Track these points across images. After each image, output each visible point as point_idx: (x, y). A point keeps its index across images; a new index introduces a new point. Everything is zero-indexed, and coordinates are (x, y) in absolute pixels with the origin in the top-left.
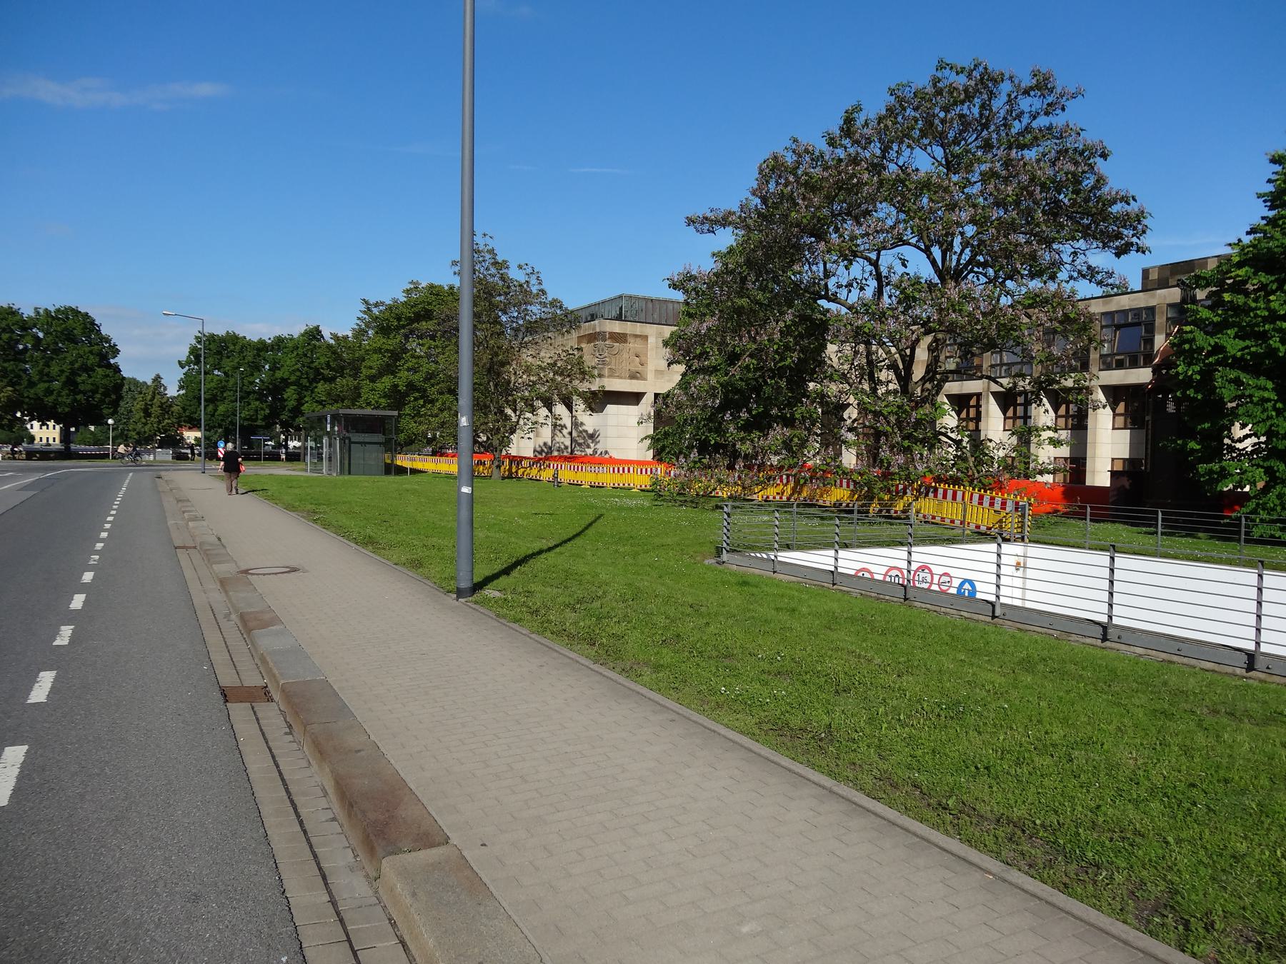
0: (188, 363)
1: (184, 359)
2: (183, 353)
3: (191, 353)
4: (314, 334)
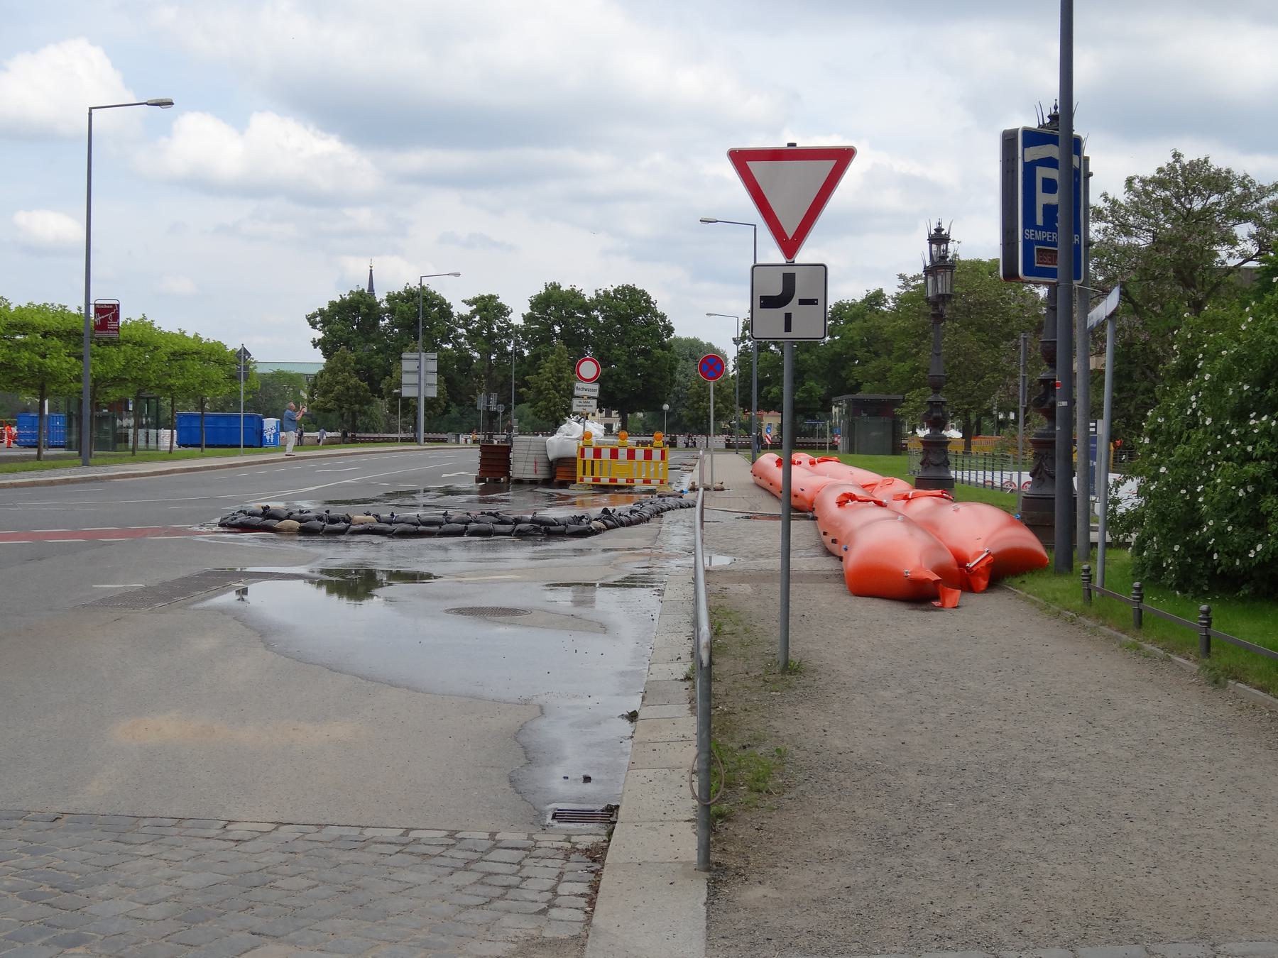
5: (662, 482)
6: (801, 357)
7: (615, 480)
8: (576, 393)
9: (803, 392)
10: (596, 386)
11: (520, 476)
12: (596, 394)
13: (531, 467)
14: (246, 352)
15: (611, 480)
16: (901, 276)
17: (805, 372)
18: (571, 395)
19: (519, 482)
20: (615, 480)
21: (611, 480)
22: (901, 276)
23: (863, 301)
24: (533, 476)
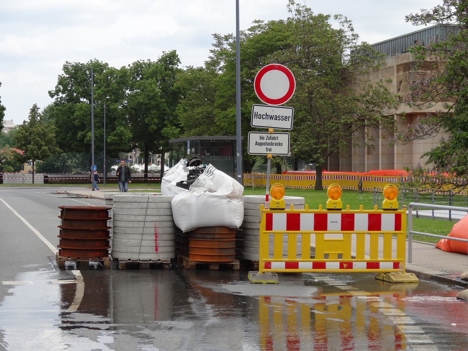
0: (57, 92)
1: (53, 89)
2: (53, 85)
3: (60, 83)
4: (171, 59)
5: (396, 265)
6: (112, 107)
7: (295, 265)
8: (256, 122)
9: (114, 135)
10: (289, 112)
11: (134, 257)
12: (288, 125)
13: (149, 242)
14: (364, 43)
15: (288, 265)
16: (216, 36)
17: (115, 119)
18: (248, 128)
19: (134, 267)
20: (295, 265)
21: (288, 265)
22: (216, 36)
23: (160, 61)
24: (153, 257)
